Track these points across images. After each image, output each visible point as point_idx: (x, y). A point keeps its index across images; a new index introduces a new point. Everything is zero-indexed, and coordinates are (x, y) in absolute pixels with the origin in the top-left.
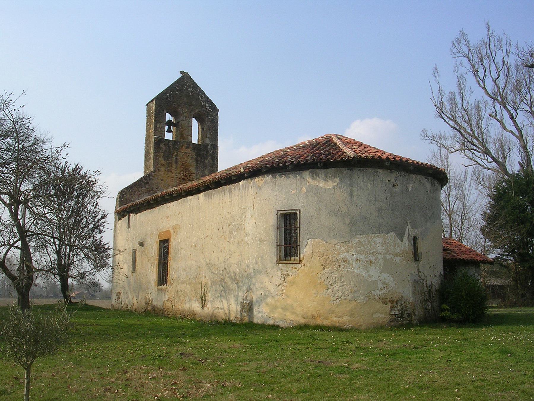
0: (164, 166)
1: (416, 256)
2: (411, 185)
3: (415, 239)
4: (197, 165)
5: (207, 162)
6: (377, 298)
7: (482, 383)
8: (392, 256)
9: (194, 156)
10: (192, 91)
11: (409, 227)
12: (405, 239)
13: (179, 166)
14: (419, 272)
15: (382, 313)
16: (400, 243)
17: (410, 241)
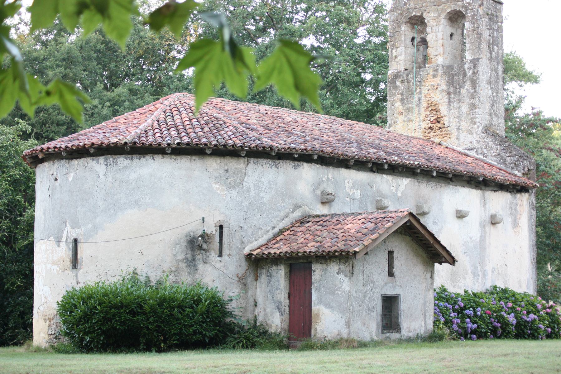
0: (401, 114)
1: (75, 263)
2: (72, 174)
3: (76, 241)
4: (449, 102)
5: (463, 91)
9: (445, 88)
11: (69, 227)
12: (63, 244)
13: (422, 110)
16: (58, 248)
17: (68, 246)
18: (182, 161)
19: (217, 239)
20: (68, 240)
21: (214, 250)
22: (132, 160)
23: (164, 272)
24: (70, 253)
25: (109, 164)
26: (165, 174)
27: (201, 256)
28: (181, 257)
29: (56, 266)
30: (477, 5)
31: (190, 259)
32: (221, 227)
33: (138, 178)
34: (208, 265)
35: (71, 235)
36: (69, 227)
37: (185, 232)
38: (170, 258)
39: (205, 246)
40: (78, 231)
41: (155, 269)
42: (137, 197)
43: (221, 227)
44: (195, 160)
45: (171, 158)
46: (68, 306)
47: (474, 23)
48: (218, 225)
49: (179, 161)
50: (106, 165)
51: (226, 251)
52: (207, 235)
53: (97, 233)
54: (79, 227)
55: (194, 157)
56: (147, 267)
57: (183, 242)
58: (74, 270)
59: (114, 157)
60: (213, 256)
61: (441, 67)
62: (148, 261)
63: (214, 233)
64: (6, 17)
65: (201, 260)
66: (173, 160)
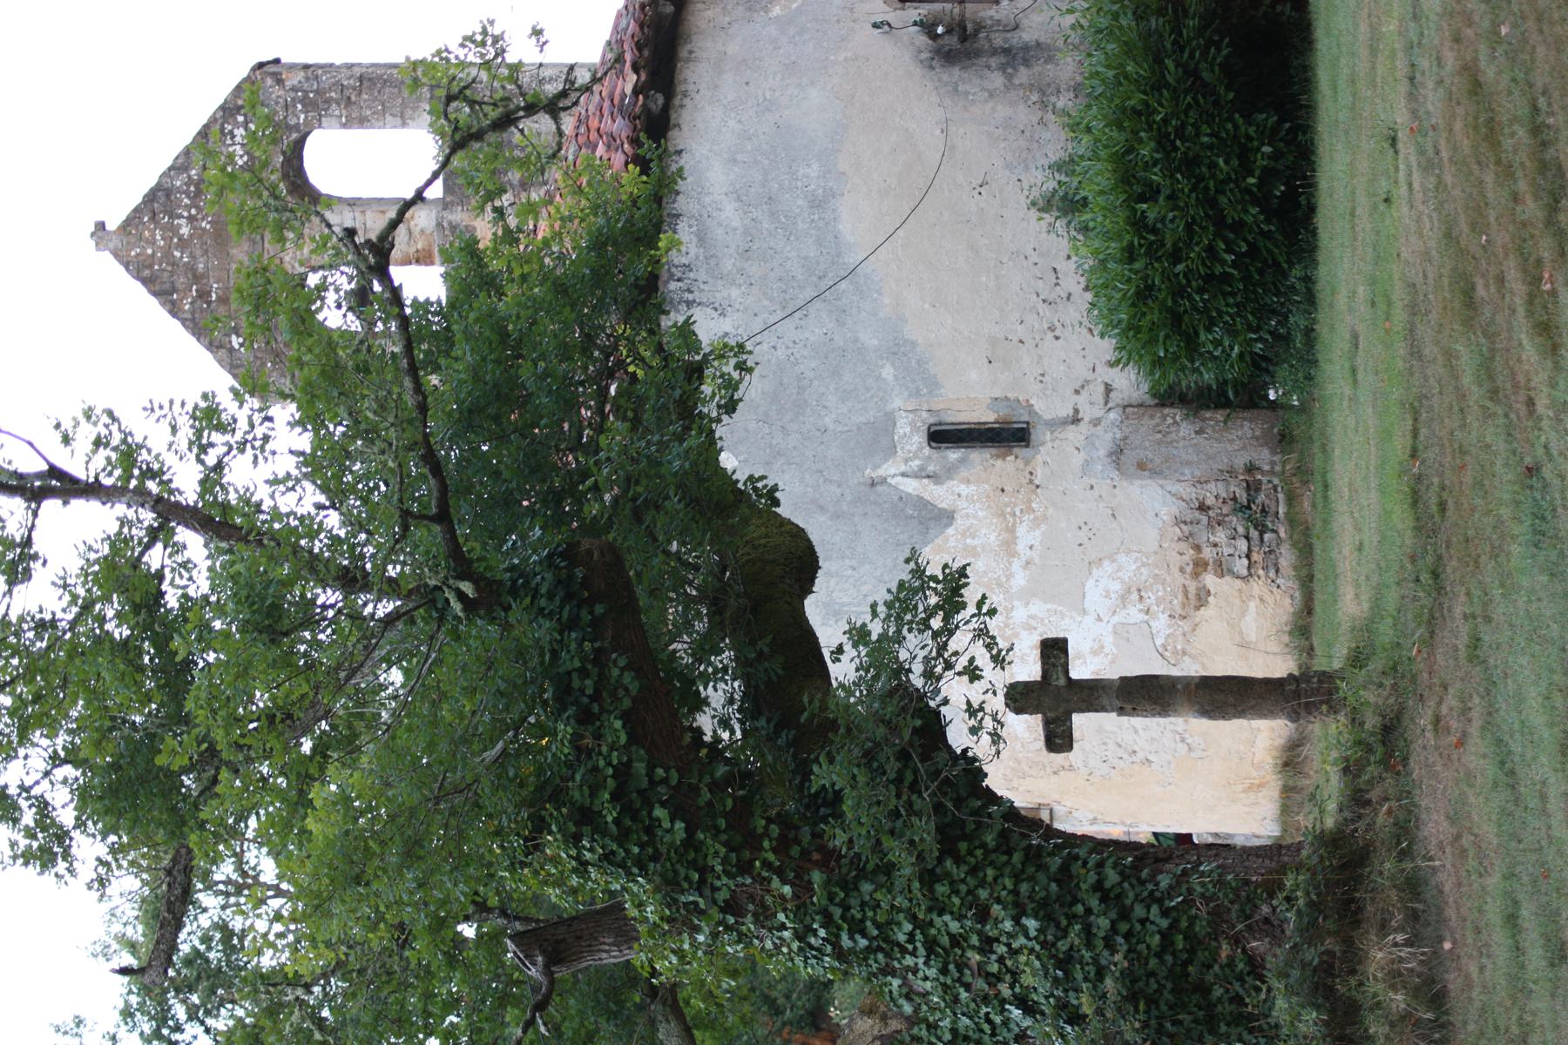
1: (1008, 435)
3: (941, 436)
6: (1185, 626)
7: (1434, 508)
8: (1016, 565)
10: (191, 219)
11: (890, 469)
12: (940, 495)
14: (1076, 420)
15: (1244, 612)
18: (691, 80)
20: (931, 468)
22: (678, 216)
23: (1041, 121)
24: (979, 457)
25: (687, 296)
26: (732, 123)
28: (997, 80)
29: (1021, 531)
30: (277, 91)
31: (1004, 60)
33: (739, 199)
35: (916, 457)
36: (890, 469)
37: (918, 71)
38: (1000, 107)
40: (903, 427)
41: (1035, 145)
42: (800, 202)
44: (691, 52)
45: (682, 106)
47: (328, 101)
49: (691, 87)
50: (689, 304)
53: (914, 344)
54: (890, 420)
55: (683, 53)
56: (1027, 168)
57: (951, 75)
58: (1035, 435)
59: (664, 276)
61: (445, 214)
62: (1009, 166)
66: (687, 101)
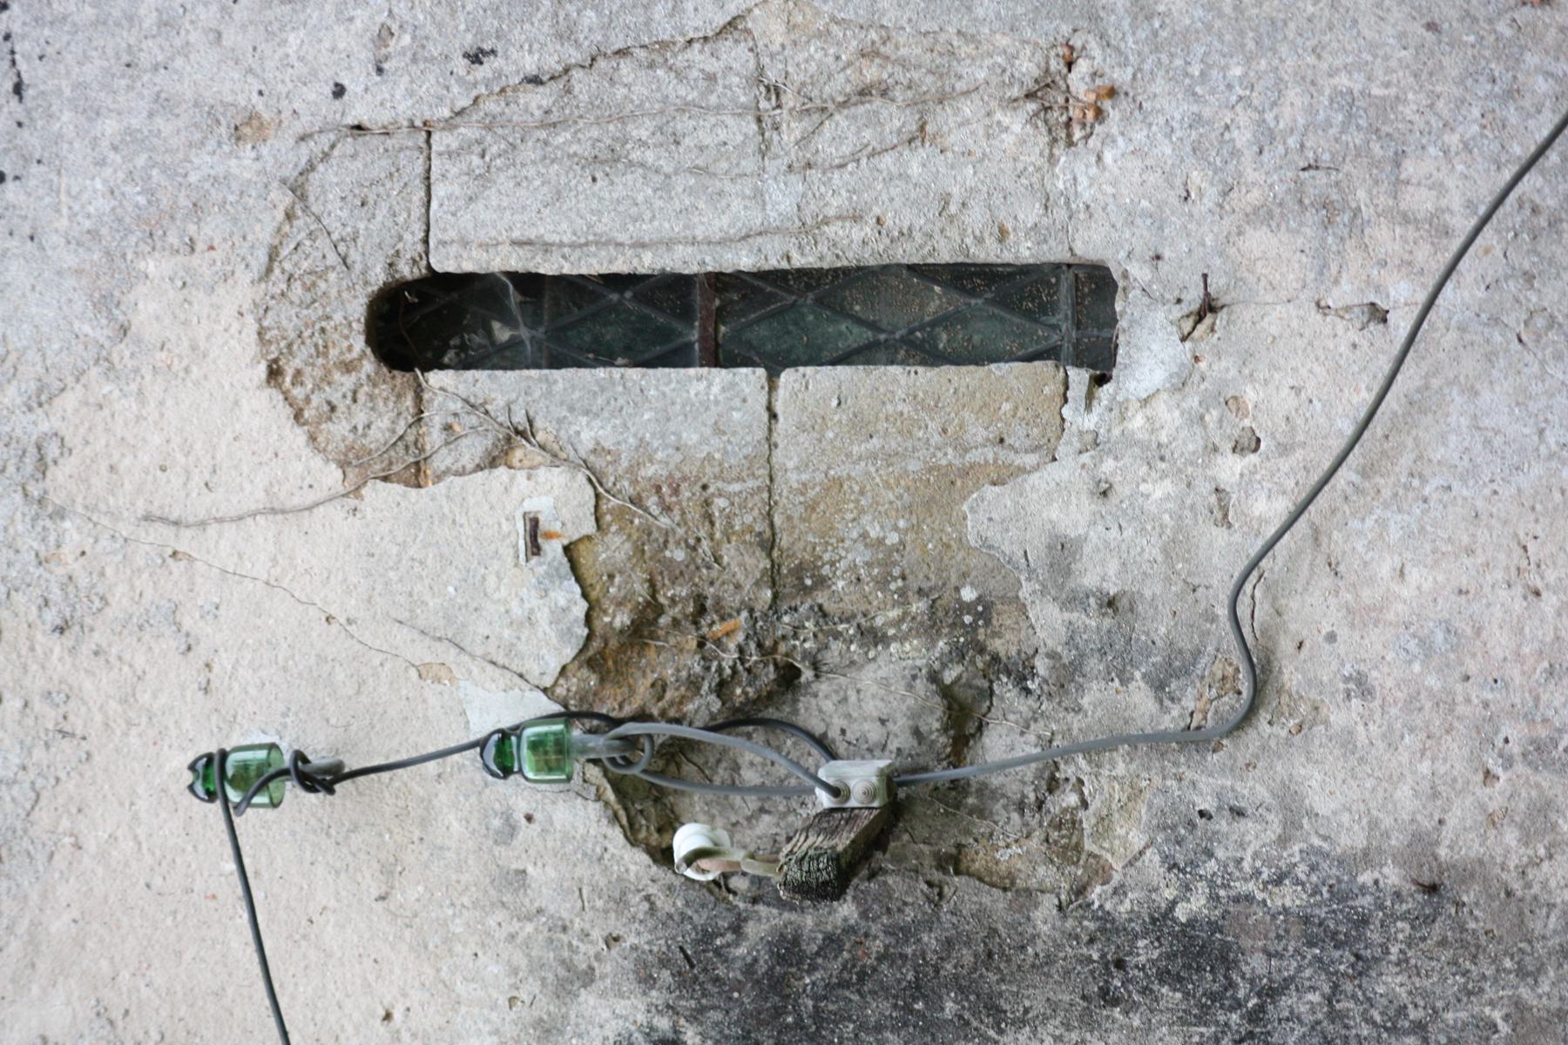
19: (691, 411)
21: (946, 487)
27: (1103, 783)
32: (423, 322)
34: (1309, 612)
39: (872, 703)
43: (423, 322)
46: (1047, 308)
48: (373, 407)
51: (976, 191)
52: (602, 655)
60: (1088, 493)
63: (557, 497)
64: (500, 320)
65: (1206, 783)
